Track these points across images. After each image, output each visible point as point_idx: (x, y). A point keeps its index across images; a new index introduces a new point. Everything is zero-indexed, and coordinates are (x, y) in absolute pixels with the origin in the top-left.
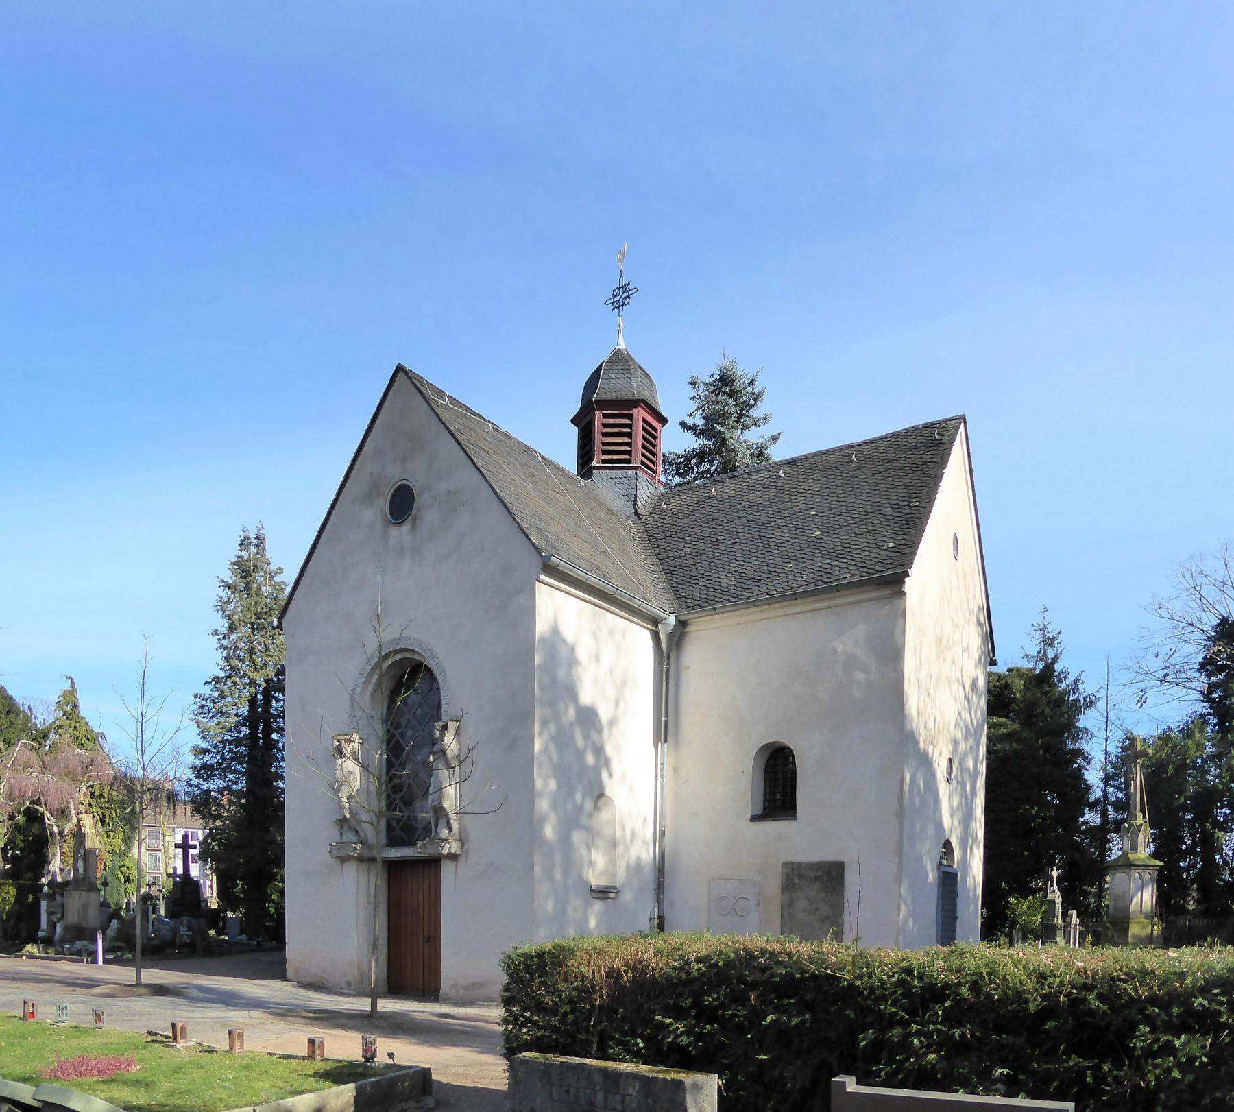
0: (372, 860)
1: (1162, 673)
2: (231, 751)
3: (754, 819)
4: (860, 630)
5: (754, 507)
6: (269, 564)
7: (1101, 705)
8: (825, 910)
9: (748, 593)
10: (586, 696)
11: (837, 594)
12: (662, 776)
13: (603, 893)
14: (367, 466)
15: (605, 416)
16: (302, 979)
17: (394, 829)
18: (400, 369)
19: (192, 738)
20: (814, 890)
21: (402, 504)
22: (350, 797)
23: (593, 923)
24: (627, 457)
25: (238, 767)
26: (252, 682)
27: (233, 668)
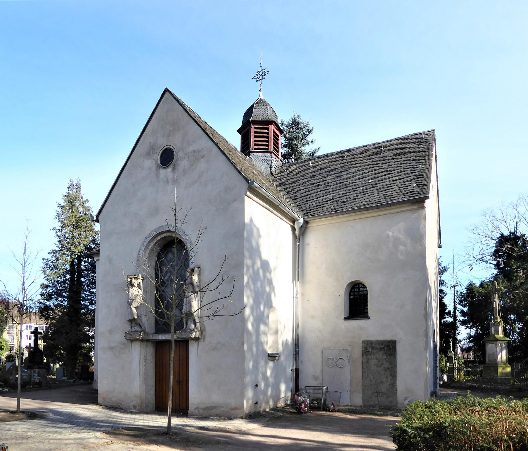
0: (148, 341)
1: (481, 256)
2: (61, 286)
3: (346, 319)
4: (402, 225)
5: (334, 170)
6: (82, 198)
7: (450, 271)
8: (386, 365)
9: (338, 209)
10: (264, 256)
11: (377, 210)
12: (297, 298)
13: (273, 357)
14: (147, 139)
15: (256, 128)
16: (107, 404)
17: (159, 325)
18: (166, 90)
19: (42, 280)
20: (380, 355)
21: (167, 158)
22: (137, 308)
23: (269, 373)
24: (266, 147)
25: (64, 294)
26: (73, 253)
27: (63, 246)
